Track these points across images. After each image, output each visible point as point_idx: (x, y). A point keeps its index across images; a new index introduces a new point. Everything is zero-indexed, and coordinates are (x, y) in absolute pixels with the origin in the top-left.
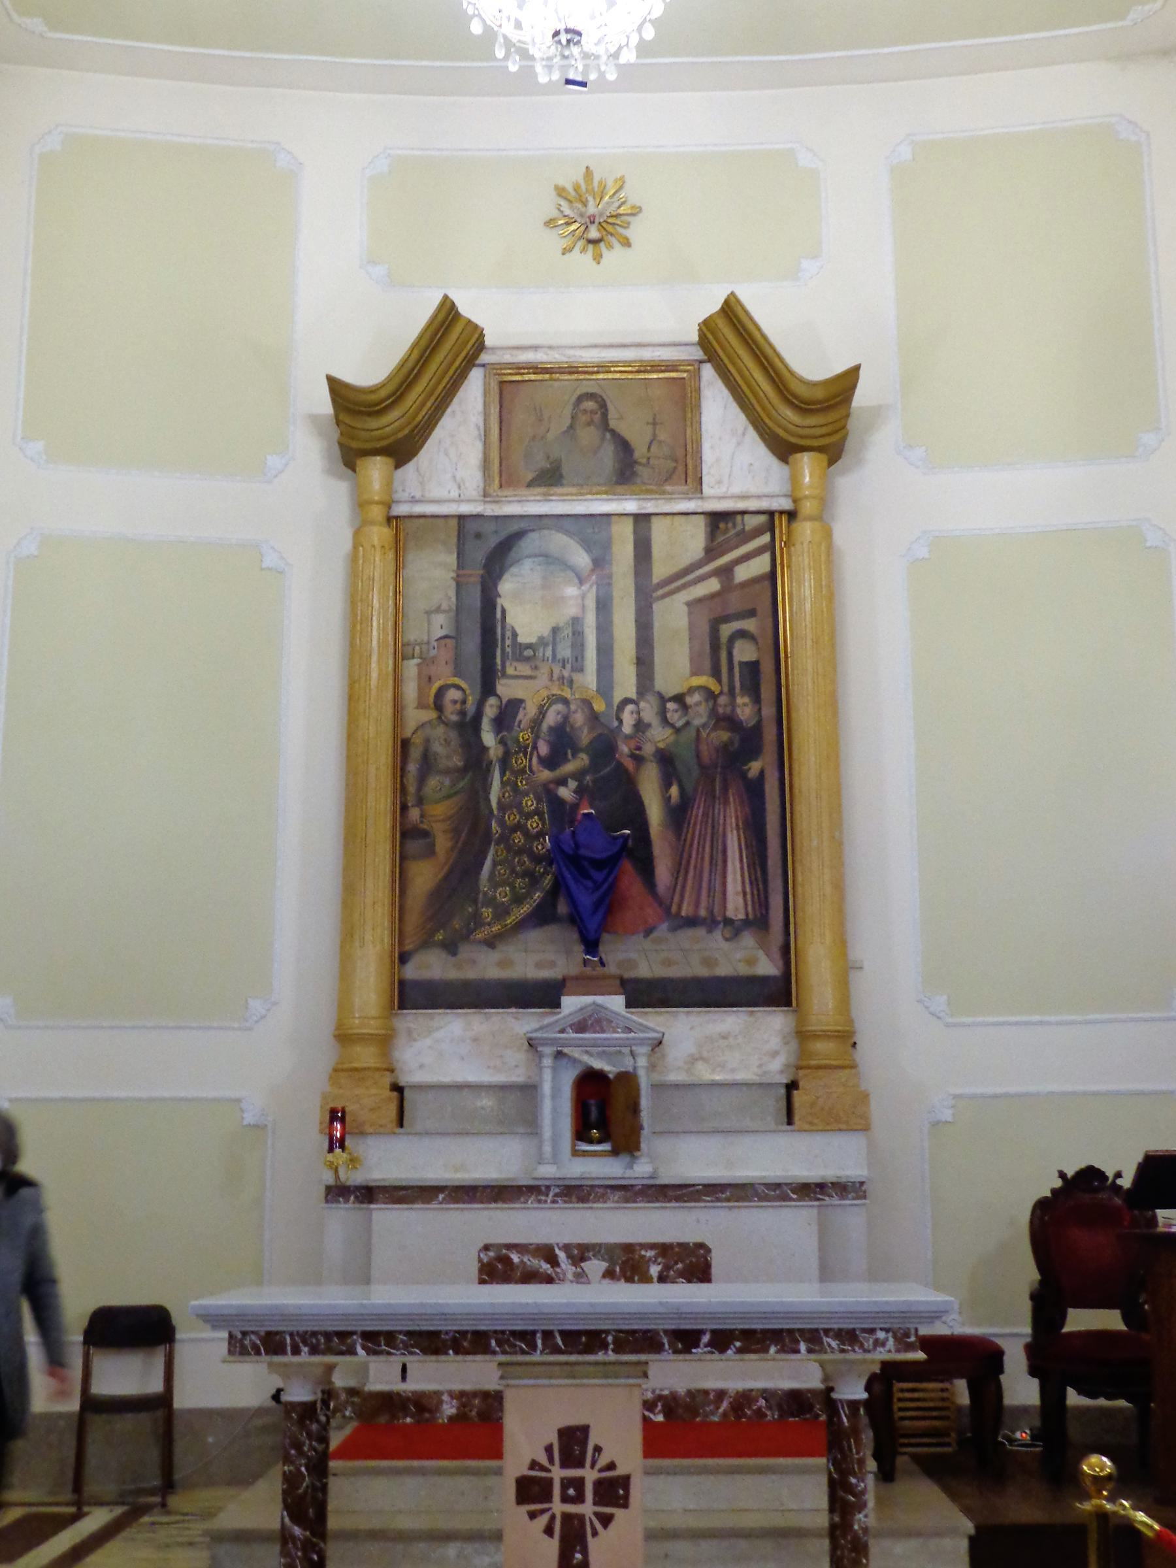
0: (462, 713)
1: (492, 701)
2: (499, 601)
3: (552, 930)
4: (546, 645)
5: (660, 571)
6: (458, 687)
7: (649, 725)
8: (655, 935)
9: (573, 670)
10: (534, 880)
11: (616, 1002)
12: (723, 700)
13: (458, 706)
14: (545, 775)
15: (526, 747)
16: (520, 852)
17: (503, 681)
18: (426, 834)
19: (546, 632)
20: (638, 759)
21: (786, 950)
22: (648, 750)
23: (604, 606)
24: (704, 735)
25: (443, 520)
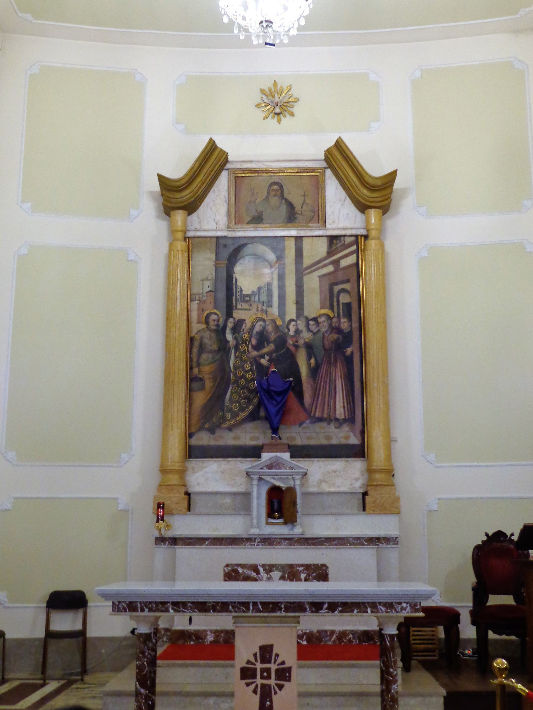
0: (217, 325)
1: (231, 320)
2: (234, 275)
3: (258, 423)
4: (255, 295)
5: (307, 262)
6: (216, 314)
7: (302, 331)
8: (304, 425)
9: (267, 306)
10: (249, 400)
11: (286, 456)
12: (334, 320)
13: (216, 322)
14: (255, 353)
15: (247, 340)
16: (243, 388)
17: (236, 311)
18: (201, 380)
19: (255, 289)
20: (297, 347)
21: (362, 432)
22: (301, 342)
23: (281, 278)
24: (326, 335)
25: (209, 239)
